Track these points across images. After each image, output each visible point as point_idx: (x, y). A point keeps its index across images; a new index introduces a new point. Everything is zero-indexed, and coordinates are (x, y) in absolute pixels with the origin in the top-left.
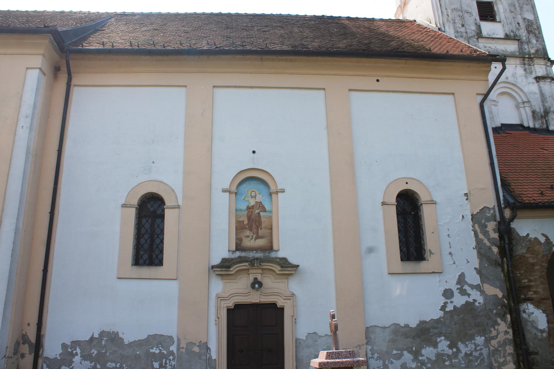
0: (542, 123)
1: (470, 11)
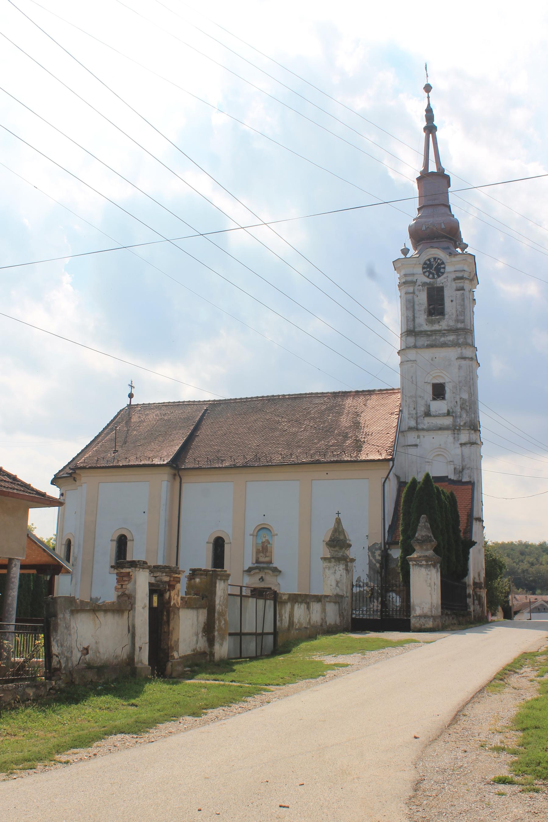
1: (422, 396)
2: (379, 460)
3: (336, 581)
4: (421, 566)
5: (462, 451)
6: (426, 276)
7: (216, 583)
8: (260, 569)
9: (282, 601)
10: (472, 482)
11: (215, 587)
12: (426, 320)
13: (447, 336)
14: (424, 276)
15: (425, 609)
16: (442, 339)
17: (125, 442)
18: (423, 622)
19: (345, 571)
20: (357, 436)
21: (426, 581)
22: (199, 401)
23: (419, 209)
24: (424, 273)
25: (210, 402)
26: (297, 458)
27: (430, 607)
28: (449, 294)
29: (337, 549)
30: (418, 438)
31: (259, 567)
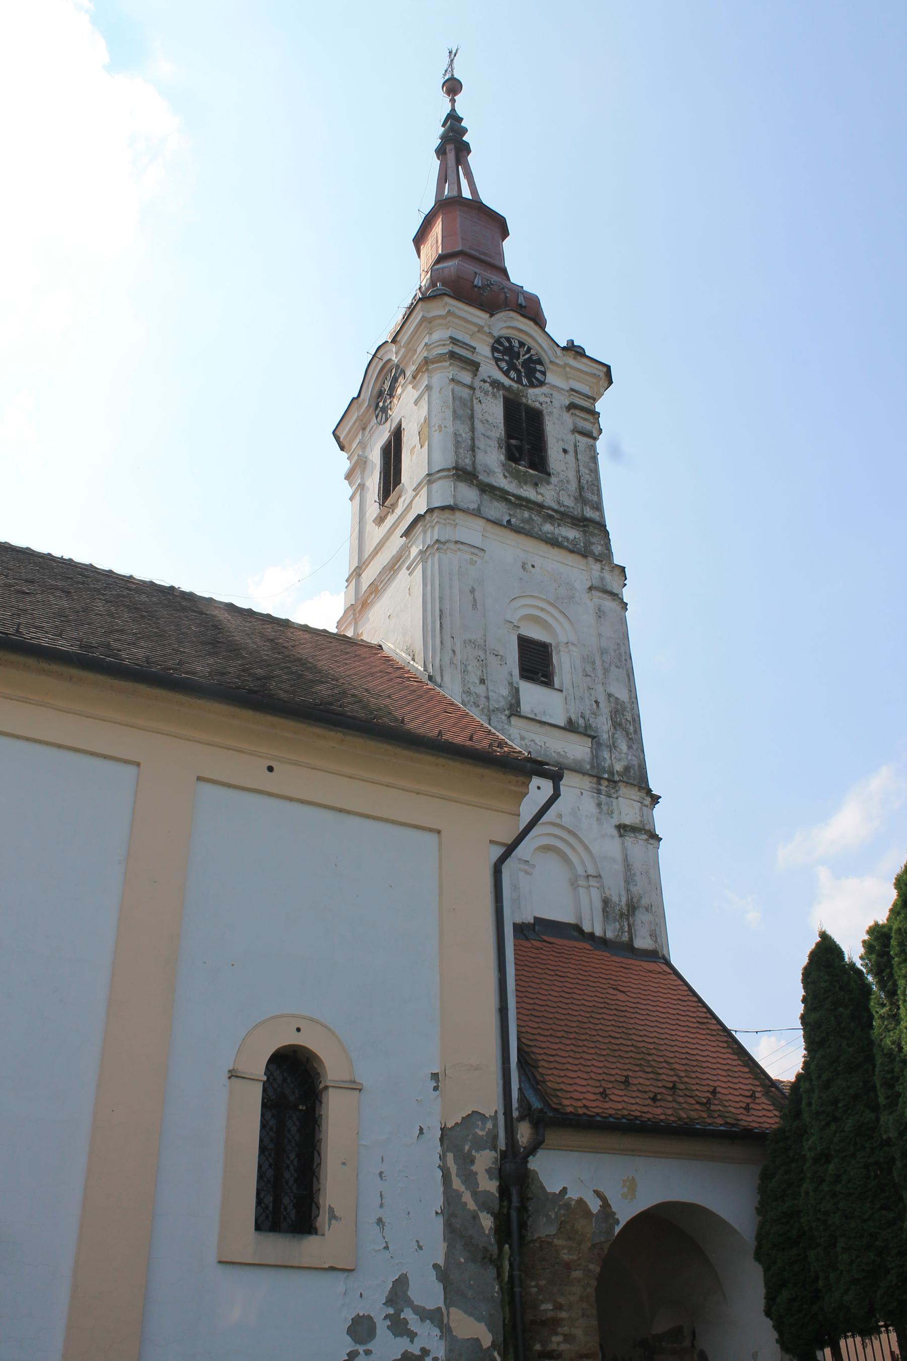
0: (622, 927)
5: (624, 850)
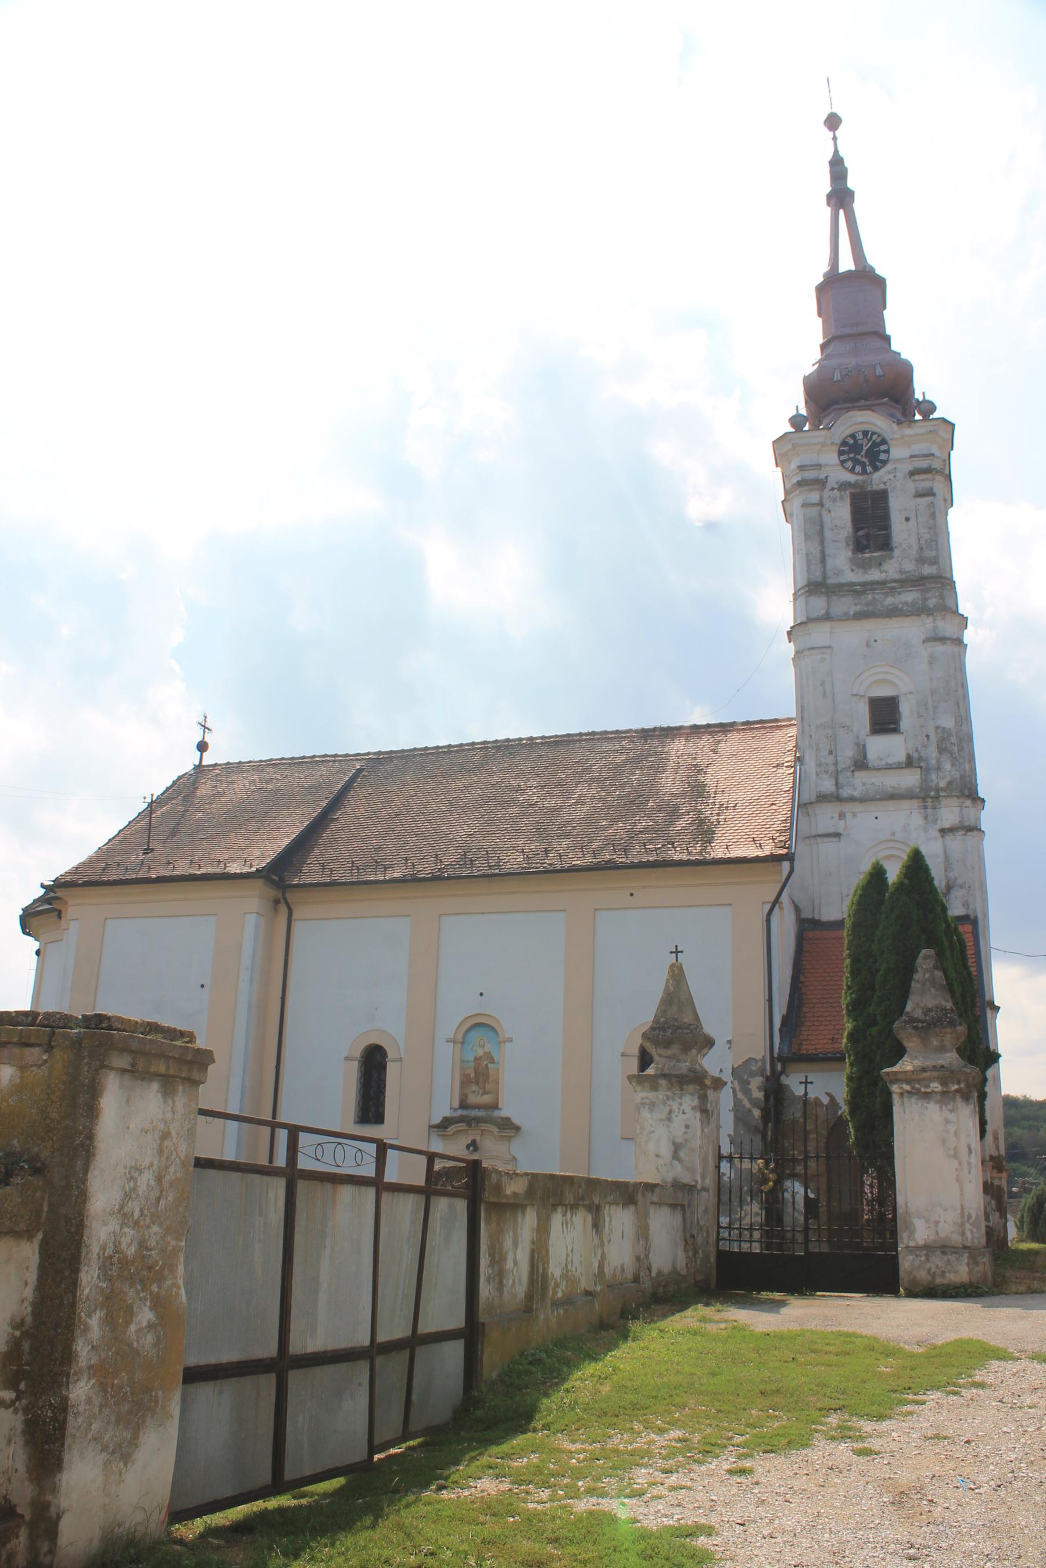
2: (757, 860)
3: (674, 1144)
4: (927, 1096)
6: (846, 469)
7: (94, 1092)
8: (470, 1122)
9: (504, 1201)
10: (972, 917)
11: (92, 1111)
12: (851, 560)
13: (899, 593)
14: (843, 470)
15: (941, 1225)
16: (889, 600)
17: (173, 834)
18: (940, 1264)
19: (698, 1115)
20: (700, 811)
21: (944, 1142)
22: (347, 755)
23: (823, 347)
24: (843, 462)
25: (370, 756)
26: (560, 859)
27: (959, 1220)
28: (898, 506)
29: (675, 1050)
30: (840, 819)
31: (467, 1116)
